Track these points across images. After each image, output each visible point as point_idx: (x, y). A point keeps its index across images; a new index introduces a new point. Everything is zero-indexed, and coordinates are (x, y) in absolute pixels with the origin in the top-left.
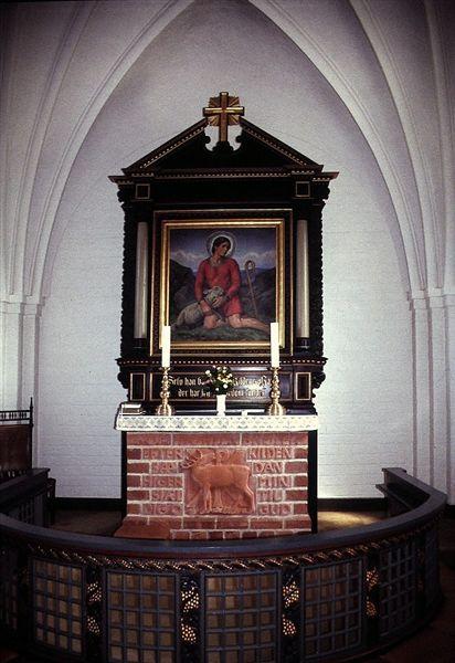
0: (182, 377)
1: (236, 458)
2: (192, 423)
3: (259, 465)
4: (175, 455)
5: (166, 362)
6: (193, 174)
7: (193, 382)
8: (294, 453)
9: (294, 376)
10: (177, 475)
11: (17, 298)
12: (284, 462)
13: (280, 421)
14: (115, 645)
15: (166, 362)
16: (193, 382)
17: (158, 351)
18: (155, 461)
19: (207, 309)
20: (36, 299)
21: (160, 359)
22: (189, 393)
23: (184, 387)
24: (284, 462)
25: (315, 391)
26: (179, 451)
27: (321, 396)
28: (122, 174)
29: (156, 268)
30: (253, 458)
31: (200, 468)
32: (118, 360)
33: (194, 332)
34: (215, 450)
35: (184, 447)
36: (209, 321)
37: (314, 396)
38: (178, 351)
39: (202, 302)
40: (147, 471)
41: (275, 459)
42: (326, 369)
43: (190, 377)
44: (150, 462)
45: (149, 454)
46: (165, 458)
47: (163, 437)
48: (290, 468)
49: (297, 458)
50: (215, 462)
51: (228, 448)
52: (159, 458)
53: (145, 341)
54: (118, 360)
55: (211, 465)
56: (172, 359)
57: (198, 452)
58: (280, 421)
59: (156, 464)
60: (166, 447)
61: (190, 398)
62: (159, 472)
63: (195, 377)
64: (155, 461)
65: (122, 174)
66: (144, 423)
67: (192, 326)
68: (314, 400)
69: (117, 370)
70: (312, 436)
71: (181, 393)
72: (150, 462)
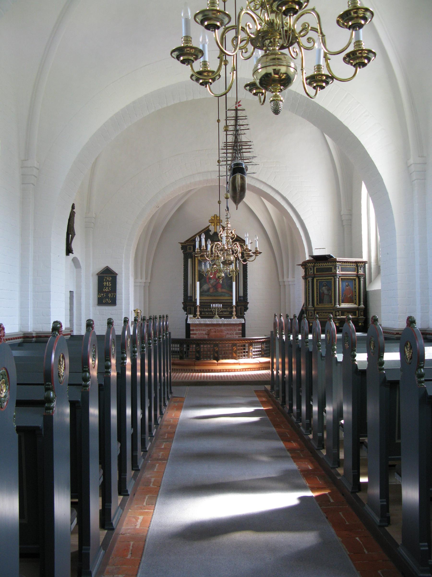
0: (203, 308)
1: (221, 331)
2: (208, 321)
3: (228, 333)
4: (204, 330)
5: (198, 303)
6: (189, 243)
7: (206, 310)
8: (238, 330)
9: (238, 308)
10: (204, 336)
11: (144, 280)
12: (235, 332)
13: (235, 320)
14: (204, 346)
15: (198, 303)
16: (206, 310)
17: (196, 300)
18: (199, 332)
19: (210, 286)
20: (149, 280)
21: (196, 302)
22: (205, 313)
23: (204, 311)
24: (235, 332)
25: (245, 312)
26: (205, 329)
27: (247, 314)
28: (334, 79)
29: (194, 265)
30: (226, 331)
31: (212, 334)
32: (183, 303)
33: (207, 294)
34: (215, 329)
35: (207, 328)
36: (211, 290)
37: (245, 314)
38: (203, 300)
39: (209, 284)
40: (196, 335)
41: (232, 331)
42: (249, 306)
43: (205, 308)
44: (197, 332)
45: (197, 330)
46: (201, 331)
47: (200, 325)
48: (237, 334)
49: (238, 331)
50: (215, 332)
51: (219, 328)
52: (200, 331)
53: (191, 297)
54: (183, 303)
55: (214, 333)
56: (200, 302)
57: (211, 329)
58: (235, 320)
59: (199, 333)
60: (202, 328)
61: (206, 315)
62: (200, 335)
63: (207, 308)
64: (199, 332)
65: (334, 79)
66: (196, 321)
67: (206, 292)
68: (244, 315)
69: (182, 306)
70: (243, 325)
71: (203, 313)
72: (197, 332)
